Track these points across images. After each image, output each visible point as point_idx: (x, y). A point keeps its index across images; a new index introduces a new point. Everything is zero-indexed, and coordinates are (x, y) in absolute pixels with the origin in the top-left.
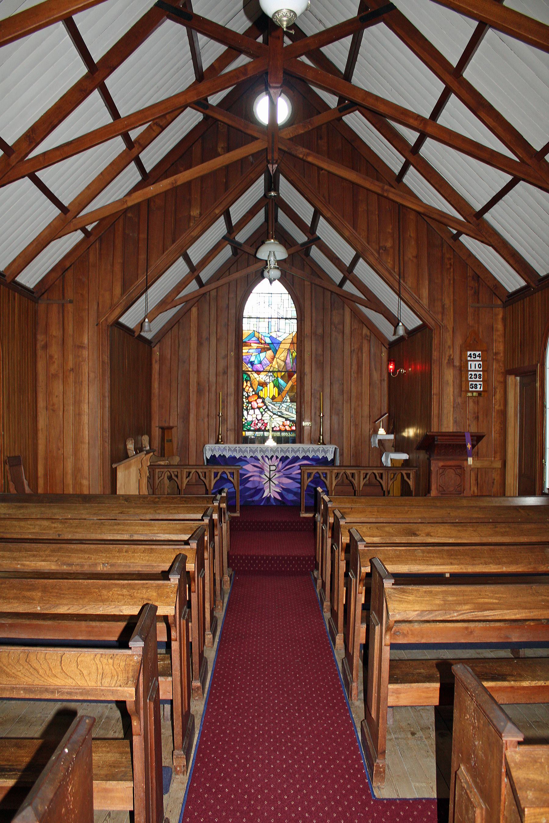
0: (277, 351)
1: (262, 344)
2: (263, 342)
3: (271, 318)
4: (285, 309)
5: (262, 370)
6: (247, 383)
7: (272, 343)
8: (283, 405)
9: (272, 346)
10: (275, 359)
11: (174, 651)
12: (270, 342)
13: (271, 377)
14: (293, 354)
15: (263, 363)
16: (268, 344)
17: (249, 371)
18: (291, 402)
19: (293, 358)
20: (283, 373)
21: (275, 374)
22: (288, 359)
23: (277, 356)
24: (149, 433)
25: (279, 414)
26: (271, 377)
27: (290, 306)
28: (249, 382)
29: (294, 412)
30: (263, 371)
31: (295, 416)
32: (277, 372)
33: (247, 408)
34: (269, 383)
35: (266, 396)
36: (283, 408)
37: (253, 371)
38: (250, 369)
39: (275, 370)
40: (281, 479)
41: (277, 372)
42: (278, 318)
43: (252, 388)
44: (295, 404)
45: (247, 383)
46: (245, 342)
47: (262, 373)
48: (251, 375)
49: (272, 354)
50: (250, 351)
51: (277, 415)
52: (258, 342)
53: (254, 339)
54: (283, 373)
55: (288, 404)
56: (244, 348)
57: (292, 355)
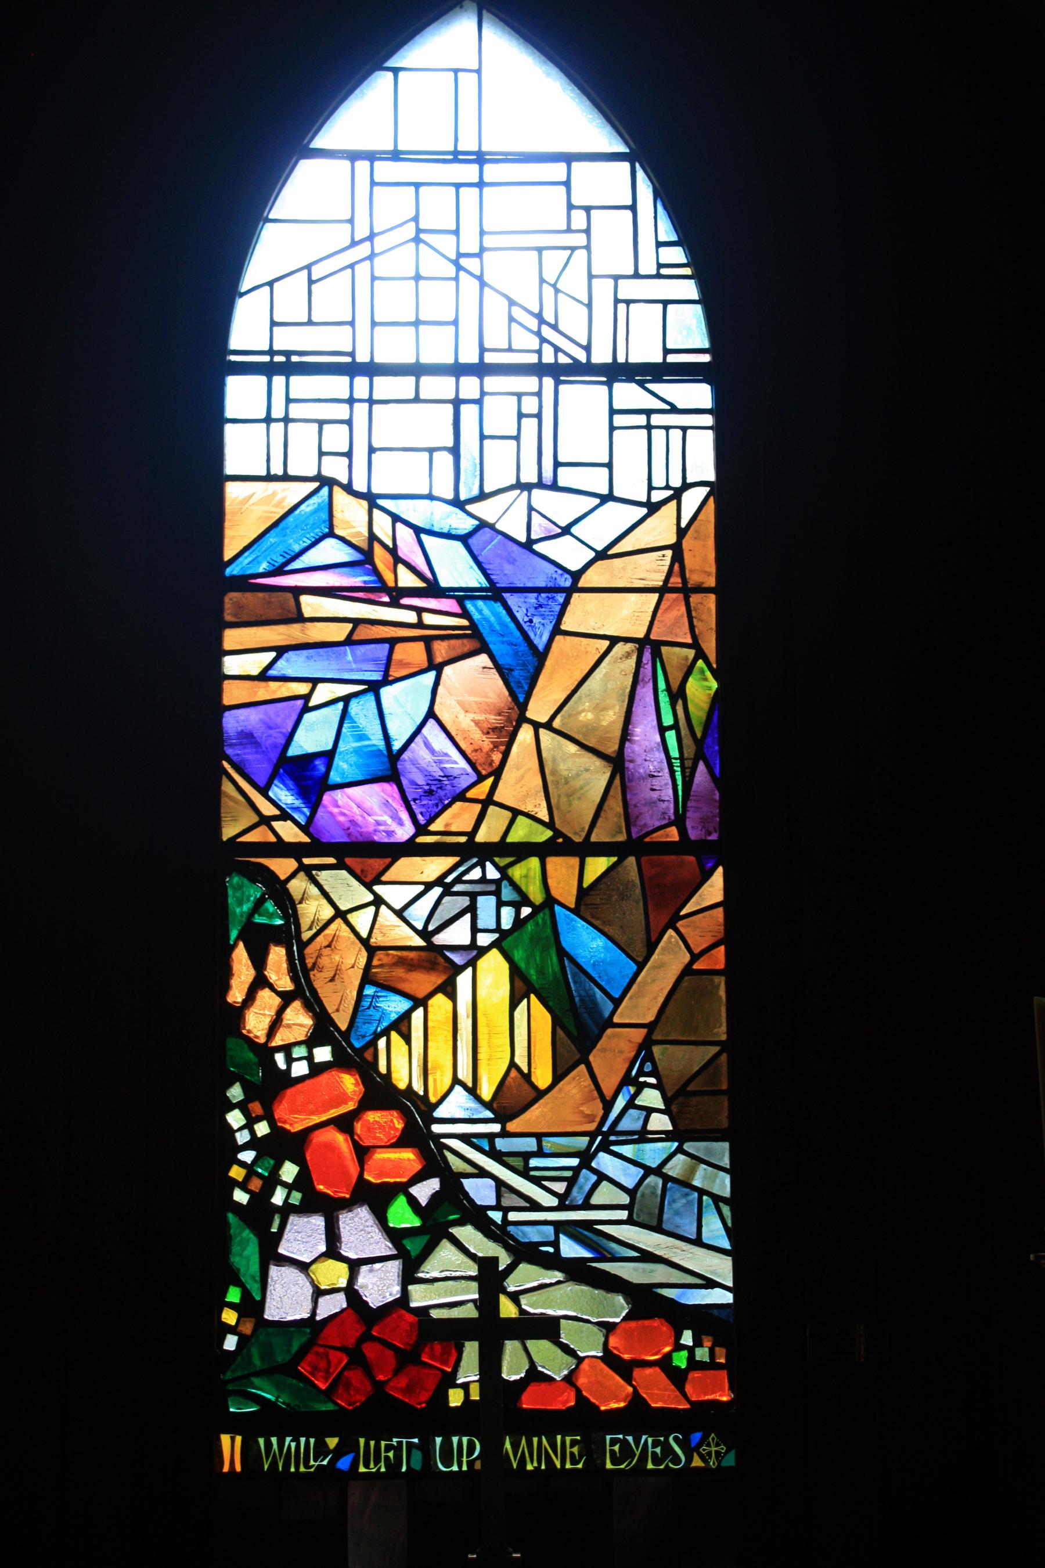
0: (541, 656)
1: (396, 596)
2: (407, 579)
3: (481, 370)
4: (603, 290)
5: (404, 832)
6: (259, 961)
7: (495, 592)
8: (604, 1162)
9: (483, 611)
10: (526, 734)
11: (583, 1193)
12: (474, 579)
13: (486, 905)
14: (693, 686)
15: (413, 775)
16: (463, 596)
17: (281, 848)
18: (678, 1135)
19: (682, 725)
20: (597, 866)
21: (527, 871)
22: (645, 732)
23: (539, 709)
24: (630, 1221)
25: (570, 1249)
26: (486, 905)
27: (648, 267)
28: (277, 955)
29: (714, 1230)
30: (411, 849)
31: (722, 1268)
32: (542, 851)
33: (261, 1199)
34: (475, 952)
35: (440, 1081)
36: (605, 1194)
37: (317, 847)
38: (289, 832)
39: (522, 832)
40: (546, 603)
41: (542, 851)
42: (539, 370)
43: (314, 1005)
44: (721, 1152)
45: (259, 961)
46: (244, 583)
47: (406, 867)
48: (298, 886)
49: (494, 687)
50: (292, 665)
51: (553, 1261)
52: (357, 579)
53: (330, 551)
54: (597, 866)
55: (653, 1153)
56: (232, 638)
57: (678, 695)
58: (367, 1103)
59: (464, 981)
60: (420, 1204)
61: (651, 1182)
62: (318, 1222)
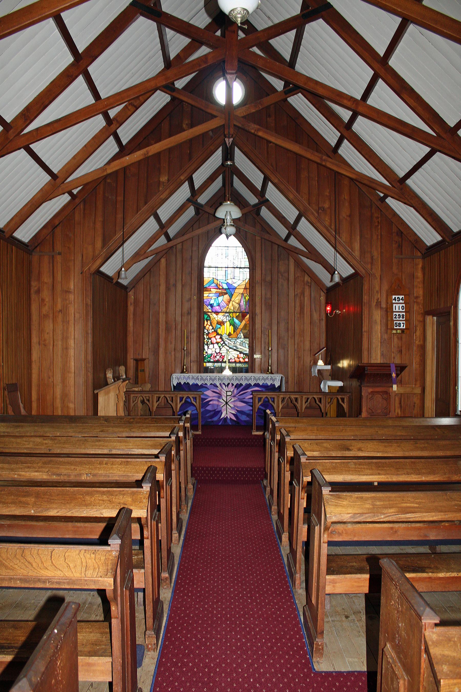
0: (232, 295)
1: (220, 289)
2: (221, 287)
3: (228, 267)
4: (239, 260)
5: (220, 311)
6: (207, 322)
7: (229, 289)
8: (237, 340)
9: (228, 291)
10: (231, 302)
12: (227, 287)
13: (227, 317)
14: (246, 298)
15: (221, 306)
16: (225, 289)
17: (209, 312)
19: (246, 301)
20: (238, 314)
21: (231, 315)
22: (242, 302)
23: (232, 300)
25: (234, 348)
26: (227, 317)
27: (243, 258)
28: (209, 321)
29: (247, 346)
30: (221, 312)
31: (248, 350)
32: (233, 313)
33: (207, 343)
34: (226, 322)
35: (223, 333)
36: (238, 343)
37: (213, 312)
38: (210, 311)
39: (231, 311)
41: (233, 313)
42: (233, 268)
43: (212, 326)
44: (248, 340)
45: (207, 322)
46: (206, 288)
47: (220, 314)
48: (211, 315)
50: (210, 295)
51: (233, 349)
52: (216, 287)
53: (213, 285)
54: (238, 314)
55: (242, 339)
57: (245, 298)
58: (217, 335)
59: (225, 324)
60: (379, 55)
61: (332, 529)
62: (212, 345)
